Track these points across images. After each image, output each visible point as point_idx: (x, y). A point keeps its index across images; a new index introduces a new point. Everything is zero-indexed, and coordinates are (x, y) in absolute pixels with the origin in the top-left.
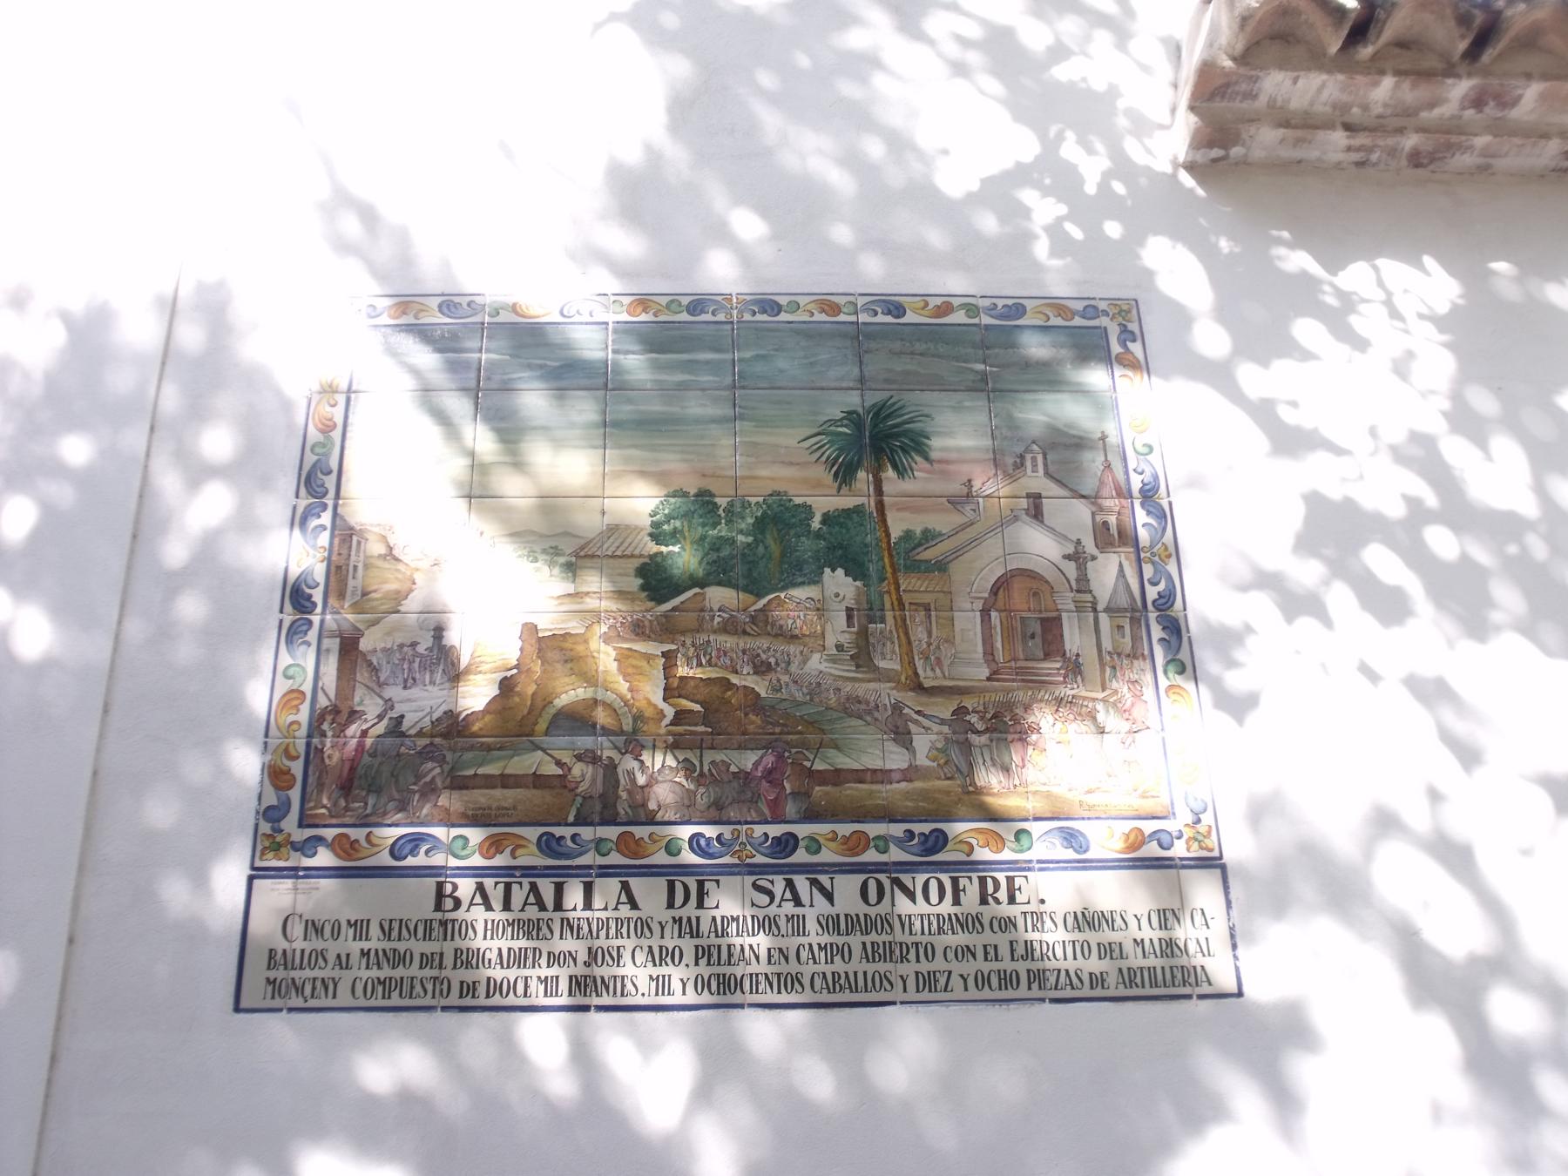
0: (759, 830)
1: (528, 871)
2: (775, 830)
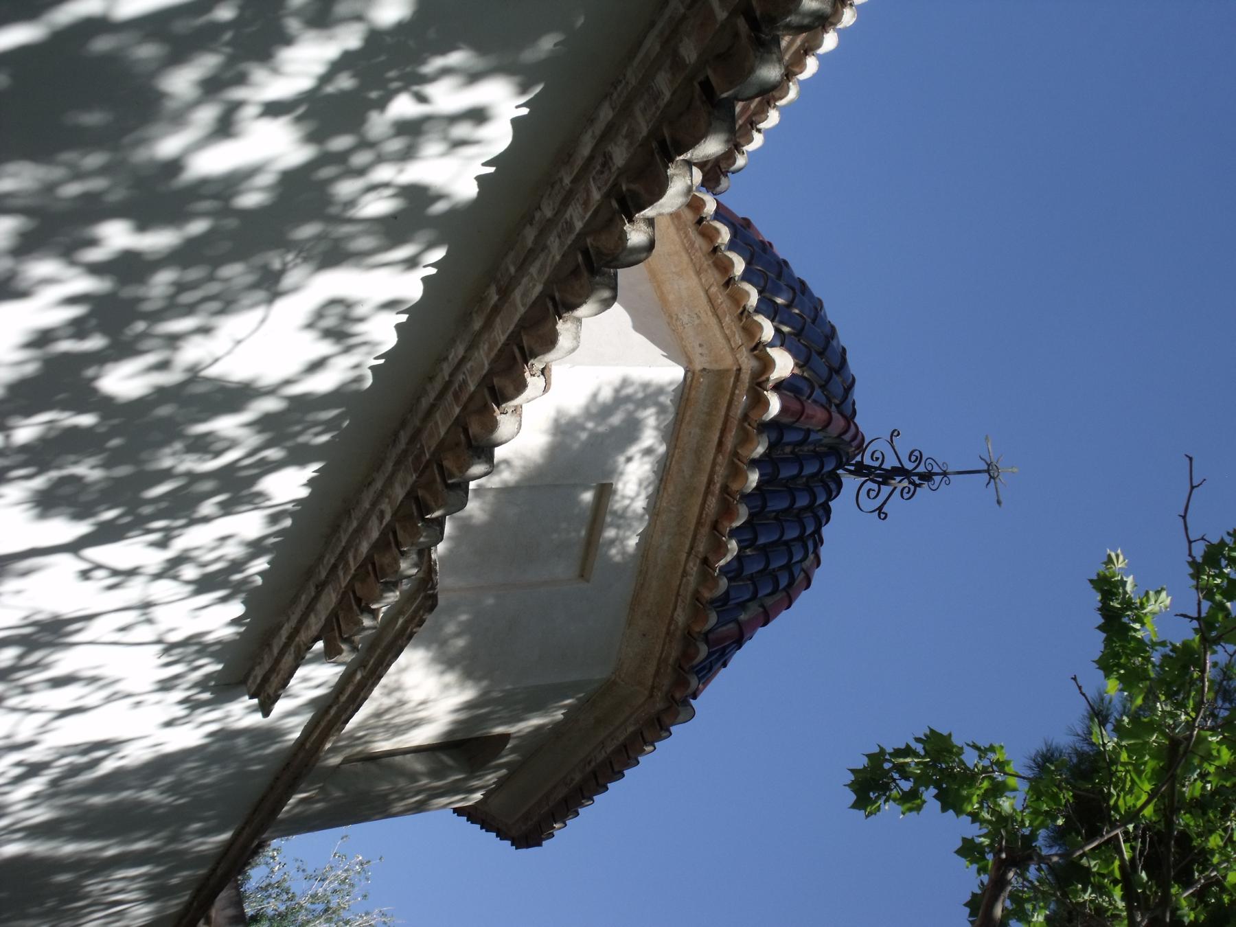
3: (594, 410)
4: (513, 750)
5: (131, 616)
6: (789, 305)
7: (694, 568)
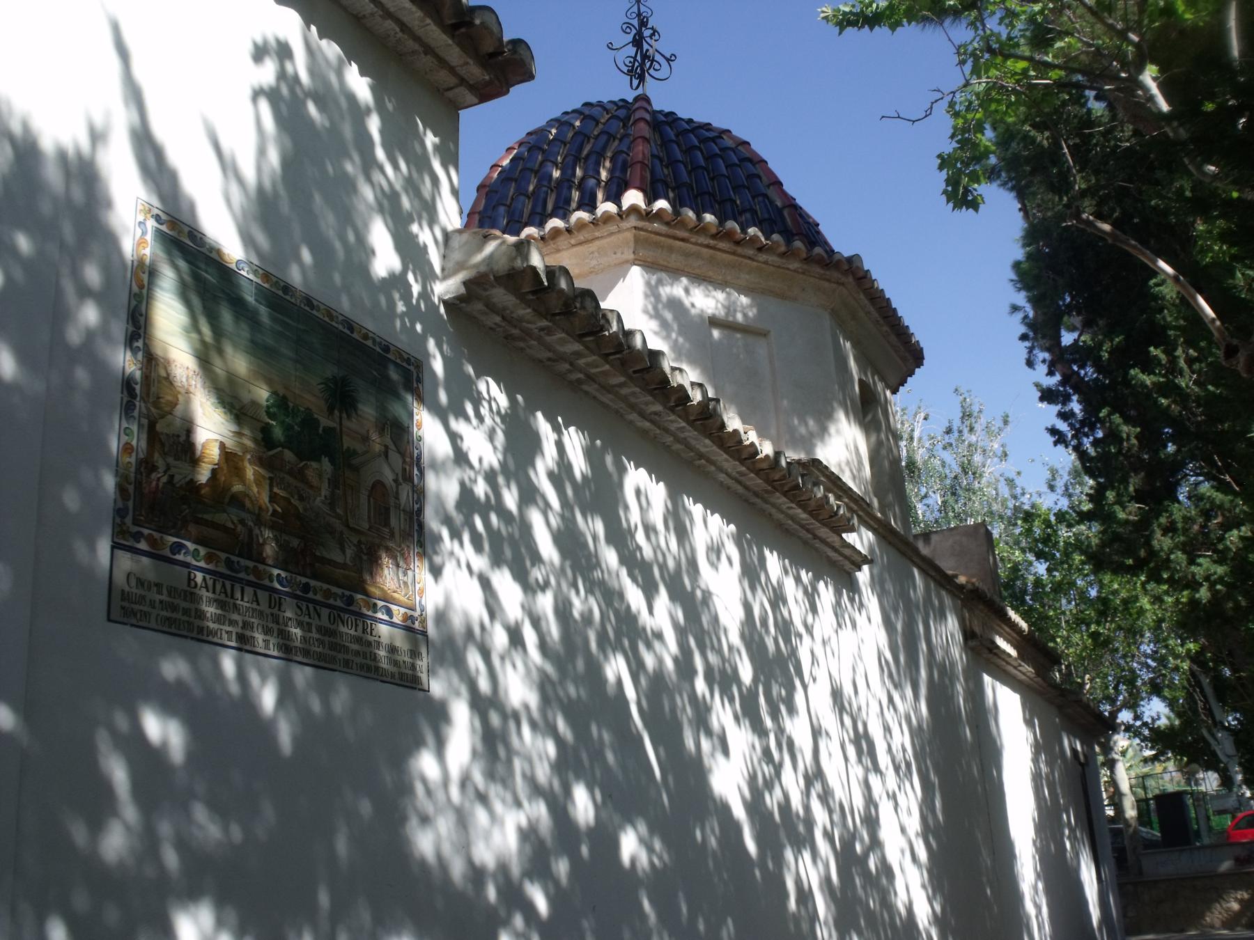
0: (299, 578)
1: (222, 575)
2: (304, 580)
3: (664, 333)
4: (866, 375)
5: (828, 649)
6: (544, 151)
7: (763, 257)
